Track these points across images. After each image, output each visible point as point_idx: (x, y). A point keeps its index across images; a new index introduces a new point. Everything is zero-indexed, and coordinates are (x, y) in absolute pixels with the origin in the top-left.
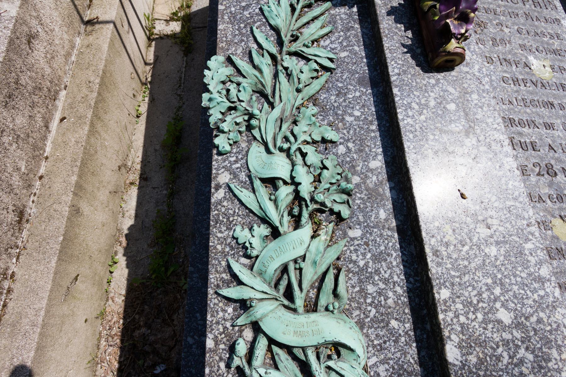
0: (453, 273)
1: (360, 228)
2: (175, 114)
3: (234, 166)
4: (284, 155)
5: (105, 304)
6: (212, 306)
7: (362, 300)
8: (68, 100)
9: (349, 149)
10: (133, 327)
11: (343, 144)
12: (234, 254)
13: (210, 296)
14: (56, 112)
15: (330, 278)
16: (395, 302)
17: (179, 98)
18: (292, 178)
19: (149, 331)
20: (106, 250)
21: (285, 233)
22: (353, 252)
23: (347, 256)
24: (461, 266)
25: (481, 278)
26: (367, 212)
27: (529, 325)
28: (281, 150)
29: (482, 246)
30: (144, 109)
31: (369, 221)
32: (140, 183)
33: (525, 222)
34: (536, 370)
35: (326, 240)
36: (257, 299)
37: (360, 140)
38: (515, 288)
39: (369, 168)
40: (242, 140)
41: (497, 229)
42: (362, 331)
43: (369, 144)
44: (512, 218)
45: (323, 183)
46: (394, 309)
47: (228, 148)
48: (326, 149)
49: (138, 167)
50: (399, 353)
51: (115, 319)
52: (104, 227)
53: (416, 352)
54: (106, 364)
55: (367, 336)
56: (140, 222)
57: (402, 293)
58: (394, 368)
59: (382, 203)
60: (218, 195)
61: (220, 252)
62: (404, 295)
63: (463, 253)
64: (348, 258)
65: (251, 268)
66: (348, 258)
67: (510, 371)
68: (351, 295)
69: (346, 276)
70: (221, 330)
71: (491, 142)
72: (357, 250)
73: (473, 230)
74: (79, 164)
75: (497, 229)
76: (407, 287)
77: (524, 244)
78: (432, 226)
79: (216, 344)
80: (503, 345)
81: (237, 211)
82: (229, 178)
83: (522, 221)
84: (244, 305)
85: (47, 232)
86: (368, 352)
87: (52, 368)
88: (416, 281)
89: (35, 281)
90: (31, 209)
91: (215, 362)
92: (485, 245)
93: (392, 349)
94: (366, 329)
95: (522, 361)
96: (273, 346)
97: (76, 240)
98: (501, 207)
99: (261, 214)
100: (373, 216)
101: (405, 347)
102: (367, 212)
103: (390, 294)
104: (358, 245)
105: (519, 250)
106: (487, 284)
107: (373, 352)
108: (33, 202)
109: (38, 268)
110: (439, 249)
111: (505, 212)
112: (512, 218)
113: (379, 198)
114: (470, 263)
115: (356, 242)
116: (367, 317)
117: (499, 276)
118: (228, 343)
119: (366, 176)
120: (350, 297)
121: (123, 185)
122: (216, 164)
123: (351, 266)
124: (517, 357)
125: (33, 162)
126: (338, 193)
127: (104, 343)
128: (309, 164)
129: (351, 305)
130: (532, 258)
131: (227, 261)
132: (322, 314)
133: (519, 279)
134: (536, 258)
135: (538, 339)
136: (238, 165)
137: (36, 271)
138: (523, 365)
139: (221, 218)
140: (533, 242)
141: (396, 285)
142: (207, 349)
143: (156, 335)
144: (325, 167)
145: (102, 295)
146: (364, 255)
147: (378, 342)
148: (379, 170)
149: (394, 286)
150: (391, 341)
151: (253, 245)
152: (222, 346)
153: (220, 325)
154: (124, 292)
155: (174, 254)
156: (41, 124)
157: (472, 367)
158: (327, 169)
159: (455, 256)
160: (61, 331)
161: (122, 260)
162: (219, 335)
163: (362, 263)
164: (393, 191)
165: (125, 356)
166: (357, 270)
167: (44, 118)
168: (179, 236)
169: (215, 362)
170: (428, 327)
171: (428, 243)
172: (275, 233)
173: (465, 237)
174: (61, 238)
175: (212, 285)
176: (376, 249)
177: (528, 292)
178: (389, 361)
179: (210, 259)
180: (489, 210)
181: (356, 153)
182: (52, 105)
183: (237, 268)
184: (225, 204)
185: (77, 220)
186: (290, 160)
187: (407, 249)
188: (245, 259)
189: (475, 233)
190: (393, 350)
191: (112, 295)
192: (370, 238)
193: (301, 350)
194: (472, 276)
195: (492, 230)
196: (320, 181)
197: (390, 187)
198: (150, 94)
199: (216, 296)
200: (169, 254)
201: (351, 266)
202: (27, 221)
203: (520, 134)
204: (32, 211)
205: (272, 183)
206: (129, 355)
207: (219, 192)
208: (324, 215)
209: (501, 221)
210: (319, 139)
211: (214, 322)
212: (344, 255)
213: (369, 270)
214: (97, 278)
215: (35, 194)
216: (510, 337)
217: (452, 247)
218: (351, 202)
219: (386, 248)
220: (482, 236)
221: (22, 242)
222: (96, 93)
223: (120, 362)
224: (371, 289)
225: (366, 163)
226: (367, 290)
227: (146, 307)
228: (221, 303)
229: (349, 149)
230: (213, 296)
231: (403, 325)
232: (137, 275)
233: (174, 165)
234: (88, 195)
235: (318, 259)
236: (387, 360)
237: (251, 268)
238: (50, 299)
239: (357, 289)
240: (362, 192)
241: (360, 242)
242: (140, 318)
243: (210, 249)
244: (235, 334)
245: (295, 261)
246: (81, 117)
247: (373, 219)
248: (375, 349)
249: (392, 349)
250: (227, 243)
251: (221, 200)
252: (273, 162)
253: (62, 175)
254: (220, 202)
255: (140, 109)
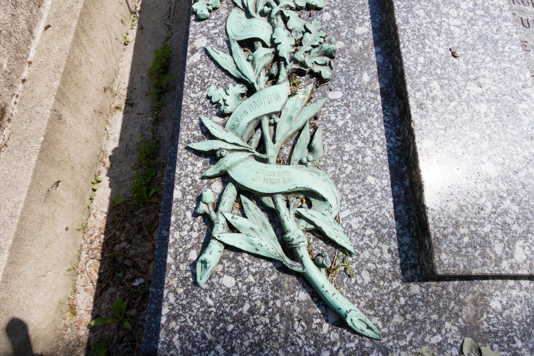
0: (437, 125)
1: (341, 90)
2: (163, 44)
3: (212, 32)
4: (264, 20)
5: (87, 220)
6: (181, 160)
7: (339, 158)
8: (53, 10)
9: (334, 16)
10: (113, 242)
11: (328, 11)
12: (207, 113)
13: (179, 151)
14: (40, 19)
15: (307, 132)
16: (373, 159)
17: (167, 28)
18: (272, 40)
19: (130, 245)
20: (89, 167)
21: (261, 89)
22: (332, 113)
23: (325, 116)
24: (447, 120)
25: (468, 131)
26: (350, 76)
27: (516, 179)
28: (262, 14)
29: (471, 103)
30: (132, 37)
31: (351, 84)
32: (125, 108)
33: (521, 84)
34: (521, 221)
35: (304, 99)
36: (227, 149)
37: (347, 8)
38: (505, 144)
39: (354, 34)
40: (222, 7)
41: (490, 88)
42: (336, 186)
43: (356, 11)
44: (507, 79)
45: (304, 46)
46: (372, 166)
47: (207, 13)
48: (310, 16)
49: (125, 93)
50: (374, 207)
51: (96, 234)
52: (87, 143)
53: (393, 207)
54: (86, 275)
55: (341, 190)
56: (125, 146)
57: (381, 152)
58: (367, 221)
59: (366, 67)
60: (193, 59)
61: (192, 111)
62: (384, 153)
63: (449, 108)
64: (326, 118)
65: (224, 125)
66: (326, 118)
67: (493, 220)
68: (327, 153)
69: (323, 134)
70: (190, 182)
71: (490, 6)
72: (336, 111)
73: (463, 88)
74: (62, 70)
75: (490, 88)
76: (387, 146)
77: (517, 104)
78: (418, 80)
79: (184, 194)
80: (487, 196)
81: (212, 73)
82: (206, 43)
83: (518, 83)
84: (213, 156)
85: (28, 131)
86: (341, 206)
87: (30, 262)
88: (397, 140)
89: (15, 177)
90: (13, 109)
91: (182, 211)
92: (475, 101)
93: (367, 203)
94: (340, 184)
95: (506, 212)
96: (241, 196)
97: (57, 146)
98: (495, 67)
99: (237, 74)
100: (356, 79)
101: (381, 201)
102: (350, 76)
103: (369, 152)
104: (337, 106)
105: (512, 109)
106: (473, 138)
107: (346, 205)
108: (15, 103)
109: (18, 164)
110: (425, 102)
111: (499, 73)
112: (507, 79)
113: (364, 62)
114: (457, 117)
115: (336, 104)
116: (343, 173)
117: (488, 132)
118: (196, 194)
119: (351, 42)
120: (326, 154)
121: (108, 108)
122: (194, 30)
123: (329, 125)
124: (502, 208)
125: (16, 63)
126: (320, 56)
127: (85, 256)
128: (290, 28)
129: (326, 162)
130: (526, 117)
131: (200, 119)
132: (295, 166)
133: (509, 136)
134: (530, 118)
135: (526, 193)
136: (217, 31)
137: (17, 167)
138: (507, 215)
139: (195, 80)
140: (528, 102)
141: (376, 144)
142: (174, 199)
143: (136, 249)
144: (308, 31)
145: (84, 209)
146: (344, 115)
147: (353, 197)
148: (366, 36)
149: (373, 145)
150: (366, 196)
151: (227, 102)
152: (190, 197)
153: (189, 178)
154: (106, 210)
155: (157, 177)
156: (24, 26)
157: (451, 213)
158: (310, 33)
159: (441, 110)
160: (40, 230)
161: (105, 181)
162: (187, 187)
163: (340, 123)
164: (379, 56)
165: (105, 268)
166: (335, 129)
167: (28, 22)
168: (162, 161)
169: (182, 211)
170: (407, 183)
171: (413, 95)
172: (251, 90)
173: (454, 93)
174: (42, 139)
175: (183, 141)
176: (357, 110)
177: (519, 149)
178: (363, 214)
179: (182, 118)
180: (482, 70)
181: (342, 19)
182: (37, 11)
183: (208, 123)
184: (201, 66)
185: (59, 126)
186: (271, 24)
187: (390, 111)
188: (219, 118)
189: (465, 90)
190: (368, 204)
191: (93, 211)
192: (351, 100)
193: (270, 199)
194: (458, 130)
195: (483, 88)
196: (301, 45)
197: (376, 52)
198: (139, 23)
199: (186, 151)
200: (152, 177)
201: (329, 125)
202: (9, 120)
203: (522, 11)
204: (14, 111)
205: (249, 44)
206: (109, 268)
207: (194, 55)
208: (304, 78)
209: (494, 81)
210: (304, 5)
211: (183, 175)
212: (323, 115)
213: (348, 130)
214: (79, 191)
215: (17, 96)
216: (495, 188)
217: (439, 102)
218: (332, 64)
219: (367, 109)
220: (473, 93)
221: (4, 139)
222: (82, 5)
223: (99, 274)
224: (348, 147)
225: (352, 29)
226: (344, 148)
227: (127, 224)
228: (190, 158)
229: (334, 16)
230: (183, 152)
231: (381, 181)
232: (119, 195)
233: (160, 93)
234: (71, 106)
235: (294, 115)
236: (361, 213)
237: (224, 125)
238: (29, 194)
239: (334, 147)
240: (345, 57)
241: (340, 103)
242: (120, 234)
243: (183, 108)
244: (204, 186)
245: (270, 116)
246: (66, 26)
247: (355, 82)
248: (349, 203)
249: (367, 203)
250: (201, 102)
251: (196, 64)
252: (253, 25)
253: (45, 80)
254: (195, 65)
255: (128, 37)
